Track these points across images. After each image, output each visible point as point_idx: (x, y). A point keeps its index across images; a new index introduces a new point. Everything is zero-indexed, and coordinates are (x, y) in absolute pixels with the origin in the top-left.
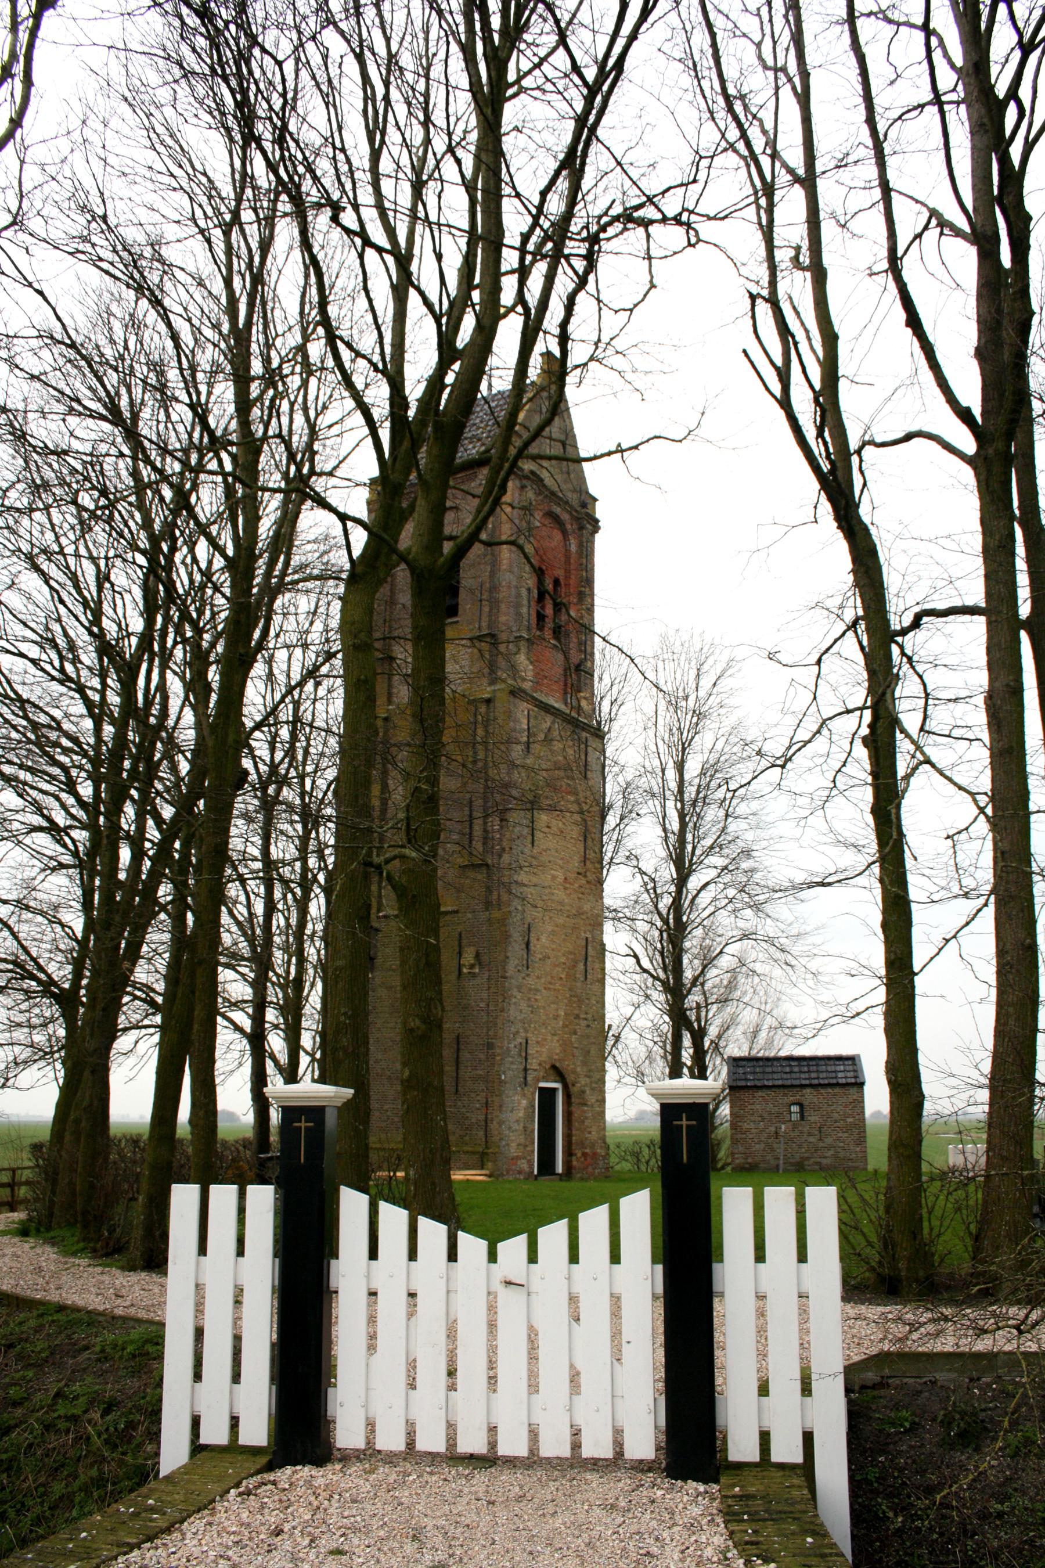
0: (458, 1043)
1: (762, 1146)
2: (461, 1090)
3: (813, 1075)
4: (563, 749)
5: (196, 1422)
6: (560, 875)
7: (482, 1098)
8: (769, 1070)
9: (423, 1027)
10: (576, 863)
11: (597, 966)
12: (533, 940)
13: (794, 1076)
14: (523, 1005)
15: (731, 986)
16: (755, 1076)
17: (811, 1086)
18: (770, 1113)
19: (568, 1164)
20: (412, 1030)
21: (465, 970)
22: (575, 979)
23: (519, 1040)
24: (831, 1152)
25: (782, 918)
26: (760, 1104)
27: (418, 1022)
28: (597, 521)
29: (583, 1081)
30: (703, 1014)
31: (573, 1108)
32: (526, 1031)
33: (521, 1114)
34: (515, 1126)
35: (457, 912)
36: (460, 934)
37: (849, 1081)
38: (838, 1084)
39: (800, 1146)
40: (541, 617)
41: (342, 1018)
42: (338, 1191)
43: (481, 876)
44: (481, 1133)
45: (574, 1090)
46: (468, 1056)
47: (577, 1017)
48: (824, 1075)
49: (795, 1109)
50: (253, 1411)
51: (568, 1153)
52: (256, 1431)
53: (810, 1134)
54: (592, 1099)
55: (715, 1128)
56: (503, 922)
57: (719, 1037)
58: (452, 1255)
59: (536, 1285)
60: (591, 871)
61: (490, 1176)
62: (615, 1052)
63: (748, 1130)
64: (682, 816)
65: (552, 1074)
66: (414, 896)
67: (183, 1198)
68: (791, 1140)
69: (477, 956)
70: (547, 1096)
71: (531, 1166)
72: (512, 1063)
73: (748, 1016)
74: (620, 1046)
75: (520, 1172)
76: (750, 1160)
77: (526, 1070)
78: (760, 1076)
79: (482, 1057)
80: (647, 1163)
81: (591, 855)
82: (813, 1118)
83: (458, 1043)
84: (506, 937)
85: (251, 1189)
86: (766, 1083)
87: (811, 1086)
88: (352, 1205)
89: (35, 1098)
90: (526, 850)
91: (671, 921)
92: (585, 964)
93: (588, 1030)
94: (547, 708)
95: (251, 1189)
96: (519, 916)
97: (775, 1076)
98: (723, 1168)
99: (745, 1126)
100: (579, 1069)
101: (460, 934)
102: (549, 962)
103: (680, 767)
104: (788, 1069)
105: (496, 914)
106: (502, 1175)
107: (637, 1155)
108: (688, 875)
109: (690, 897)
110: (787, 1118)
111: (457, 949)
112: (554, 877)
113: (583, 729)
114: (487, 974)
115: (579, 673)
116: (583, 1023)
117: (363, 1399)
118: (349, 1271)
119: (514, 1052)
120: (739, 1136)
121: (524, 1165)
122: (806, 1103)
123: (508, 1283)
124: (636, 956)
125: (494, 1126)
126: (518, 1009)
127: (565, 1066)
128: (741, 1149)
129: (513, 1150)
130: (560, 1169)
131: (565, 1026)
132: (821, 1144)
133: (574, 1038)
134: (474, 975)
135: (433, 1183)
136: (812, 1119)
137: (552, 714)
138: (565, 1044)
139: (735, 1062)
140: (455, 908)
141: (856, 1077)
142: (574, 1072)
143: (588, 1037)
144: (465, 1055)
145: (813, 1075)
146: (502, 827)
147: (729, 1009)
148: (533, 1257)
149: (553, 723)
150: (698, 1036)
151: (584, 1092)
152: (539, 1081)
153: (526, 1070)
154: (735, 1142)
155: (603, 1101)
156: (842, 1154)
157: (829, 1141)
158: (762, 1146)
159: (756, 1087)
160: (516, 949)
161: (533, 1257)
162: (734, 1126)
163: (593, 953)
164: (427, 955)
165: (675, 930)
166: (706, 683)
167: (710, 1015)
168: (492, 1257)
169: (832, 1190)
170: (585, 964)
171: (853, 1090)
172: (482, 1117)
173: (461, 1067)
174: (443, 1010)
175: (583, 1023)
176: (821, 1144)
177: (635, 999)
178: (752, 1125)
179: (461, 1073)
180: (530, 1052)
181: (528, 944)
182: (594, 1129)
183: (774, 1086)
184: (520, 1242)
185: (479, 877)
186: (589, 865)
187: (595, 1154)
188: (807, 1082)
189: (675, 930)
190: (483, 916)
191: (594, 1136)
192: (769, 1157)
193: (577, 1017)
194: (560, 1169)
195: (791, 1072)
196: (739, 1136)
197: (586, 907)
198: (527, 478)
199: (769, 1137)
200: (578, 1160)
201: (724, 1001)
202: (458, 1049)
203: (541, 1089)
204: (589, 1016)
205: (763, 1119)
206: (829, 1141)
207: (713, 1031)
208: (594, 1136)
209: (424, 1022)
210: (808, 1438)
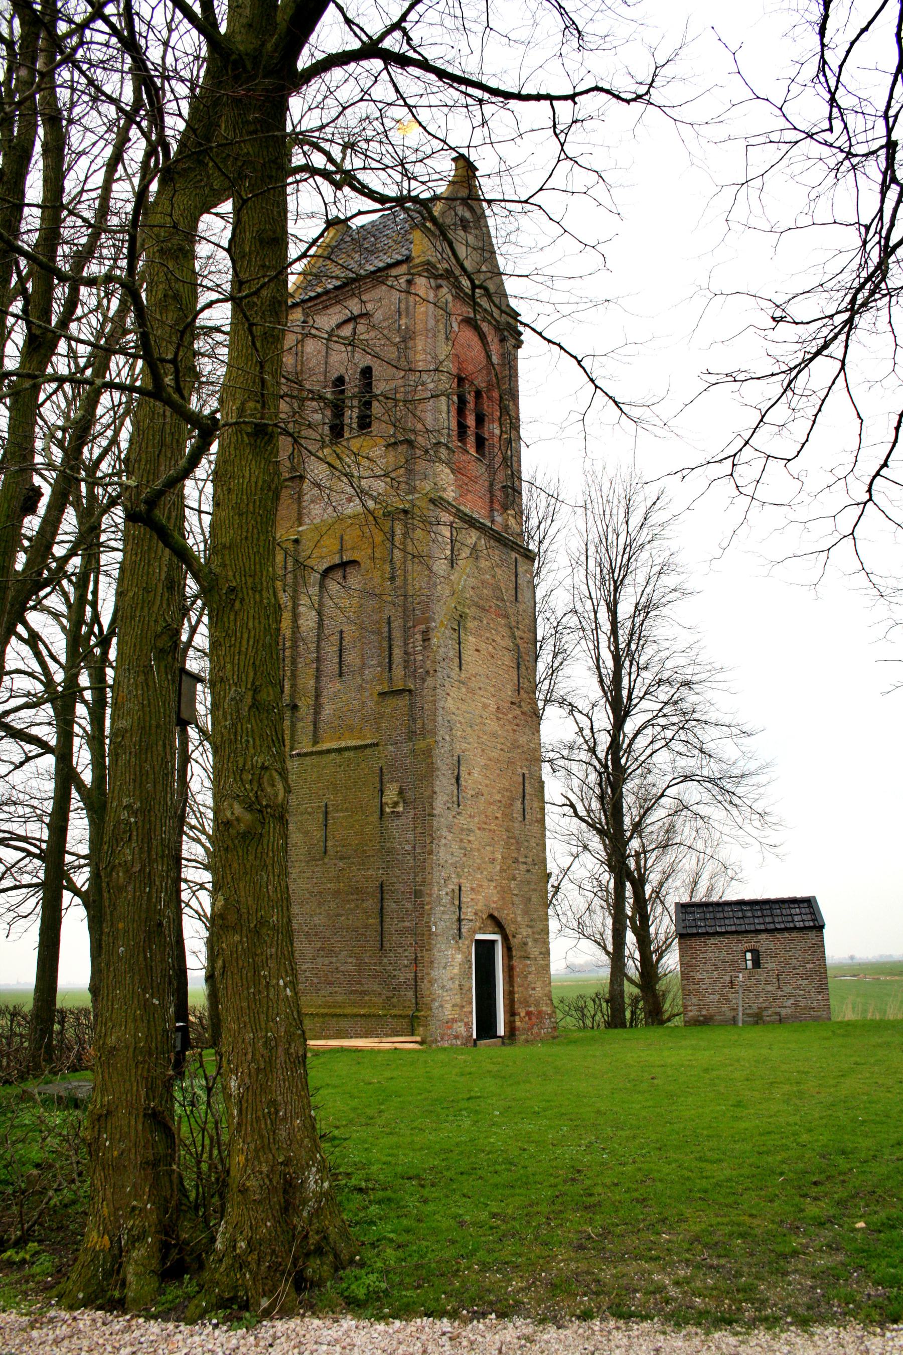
0: (382, 892)
1: (717, 997)
2: (387, 945)
3: (768, 920)
4: (493, 564)
6: (492, 704)
7: (410, 953)
8: (721, 915)
9: (248, 817)
10: (509, 692)
11: (536, 805)
12: (463, 774)
13: (747, 921)
14: (455, 846)
15: (670, 830)
16: (703, 921)
17: (766, 931)
19: (512, 1030)
20: (228, 824)
21: (388, 810)
22: (512, 819)
23: (451, 887)
24: (791, 1001)
25: (725, 757)
26: (714, 951)
27: (238, 809)
28: (522, 342)
29: (525, 931)
30: (642, 862)
31: (515, 962)
32: (459, 876)
33: (456, 971)
34: (449, 985)
35: (376, 745)
36: (381, 769)
37: (807, 924)
38: (795, 928)
39: (757, 996)
40: (462, 428)
41: (124, 815)
43: (402, 702)
44: (411, 994)
45: (514, 942)
46: (394, 906)
47: (516, 861)
48: (780, 919)
49: (749, 956)
51: (511, 1012)
53: (767, 983)
54: (534, 950)
55: (660, 979)
56: (428, 753)
57: (661, 884)
60: (525, 705)
61: (421, 1043)
62: (554, 901)
63: (701, 980)
64: (617, 658)
66: (232, 590)
69: (401, 792)
70: (485, 950)
72: (443, 912)
73: (688, 863)
74: (560, 896)
75: (456, 1037)
76: (704, 1012)
77: (459, 920)
78: (712, 923)
79: (409, 906)
80: (593, 1017)
81: (525, 684)
82: (769, 964)
83: (382, 892)
84: (432, 769)
86: (718, 929)
89: (22, 976)
90: (452, 674)
91: (609, 763)
92: (523, 803)
93: (528, 876)
94: (471, 522)
96: (447, 747)
97: (727, 922)
98: (669, 1020)
100: (519, 919)
101: (381, 769)
103: (613, 611)
104: (740, 914)
105: (421, 745)
106: (436, 1041)
107: (581, 1009)
108: (627, 714)
109: (627, 741)
110: (743, 966)
111: (378, 785)
112: (485, 706)
113: (513, 549)
114: (412, 812)
115: (508, 490)
116: (523, 868)
119: (446, 900)
120: (692, 987)
121: (460, 1028)
122: (762, 950)
124: (572, 806)
125: (424, 985)
126: (447, 851)
128: (694, 1000)
129: (448, 1012)
130: (501, 1031)
131: (502, 870)
132: (780, 993)
133: (513, 884)
134: (398, 815)
135: (273, 1103)
136: (770, 966)
137: (477, 529)
138: (504, 891)
139: (683, 908)
140: (375, 741)
141: (813, 920)
142: (514, 922)
143: (529, 883)
144: (390, 906)
145: (768, 920)
146: (425, 648)
147: (671, 855)
149: (479, 538)
150: (639, 884)
151: (525, 944)
152: (475, 932)
153: (459, 920)
154: (687, 993)
155: (547, 953)
156: (802, 1003)
157: (787, 989)
158: (717, 997)
159: (707, 934)
160: (443, 785)
162: (685, 976)
163: (529, 794)
164: (256, 691)
165: (613, 775)
166: (636, 519)
167: (649, 864)
171: (812, 934)
172: (411, 976)
173: (387, 920)
174: (288, 790)
175: (523, 868)
176: (780, 993)
177: (574, 850)
178: (705, 975)
179: (386, 927)
180: (463, 899)
181: (458, 779)
182: (538, 985)
183: (727, 932)
185: (401, 703)
186: (524, 695)
187: (540, 1012)
188: (762, 927)
189: (613, 775)
190: (406, 747)
191: (539, 992)
192: (725, 1008)
193: (516, 861)
195: (743, 917)
196: (692, 987)
197: (522, 740)
198: (441, 276)
199: (724, 987)
200: (521, 1020)
201: (664, 847)
202: (382, 899)
203: (478, 942)
204: (529, 860)
205: (717, 968)
206: (787, 989)
207: (654, 878)
208: (539, 992)
209: (249, 808)
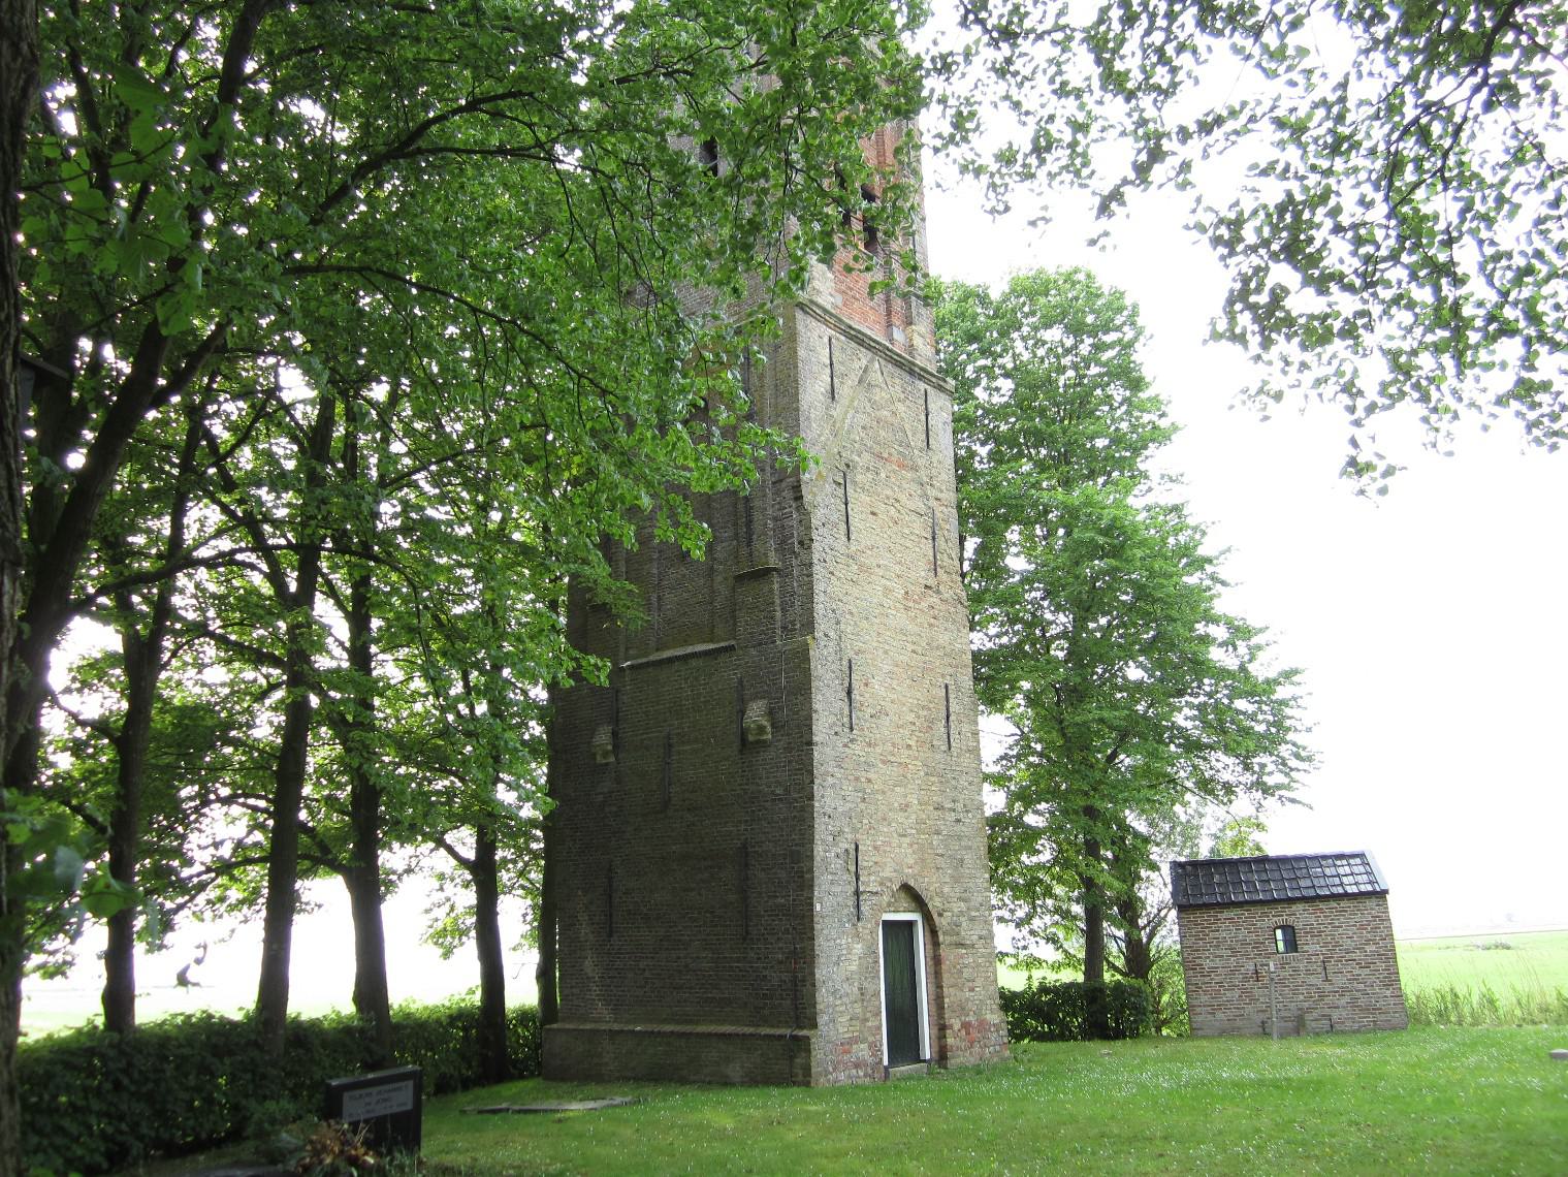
14: (848, 788)
17: (1304, 899)
18: (1244, 943)
24: (1347, 999)
26: (1230, 928)
31: (943, 951)
32: (855, 830)
37: (1363, 888)
38: (1346, 896)
42: (32, 1051)
51: (942, 1029)
63: (1214, 970)
65: (905, 902)
68: (1281, 982)
70: (900, 935)
71: (875, 1048)
77: (857, 893)
82: (1309, 945)
87: (1304, 899)
92: (948, 726)
93: (958, 828)
94: (859, 339)
99: (1207, 964)
102: (885, 721)
112: (887, 591)
116: (952, 816)
121: (862, 1051)
122: (1299, 926)
127: (927, 885)
136: (1311, 948)
137: (869, 348)
143: (960, 838)
149: (871, 361)
157: (1340, 981)
169: (292, 1010)
170: (948, 726)
171: (1371, 903)
175: (952, 816)
199: (1246, 979)
203: (885, 923)
204: (959, 806)
205: (1234, 952)
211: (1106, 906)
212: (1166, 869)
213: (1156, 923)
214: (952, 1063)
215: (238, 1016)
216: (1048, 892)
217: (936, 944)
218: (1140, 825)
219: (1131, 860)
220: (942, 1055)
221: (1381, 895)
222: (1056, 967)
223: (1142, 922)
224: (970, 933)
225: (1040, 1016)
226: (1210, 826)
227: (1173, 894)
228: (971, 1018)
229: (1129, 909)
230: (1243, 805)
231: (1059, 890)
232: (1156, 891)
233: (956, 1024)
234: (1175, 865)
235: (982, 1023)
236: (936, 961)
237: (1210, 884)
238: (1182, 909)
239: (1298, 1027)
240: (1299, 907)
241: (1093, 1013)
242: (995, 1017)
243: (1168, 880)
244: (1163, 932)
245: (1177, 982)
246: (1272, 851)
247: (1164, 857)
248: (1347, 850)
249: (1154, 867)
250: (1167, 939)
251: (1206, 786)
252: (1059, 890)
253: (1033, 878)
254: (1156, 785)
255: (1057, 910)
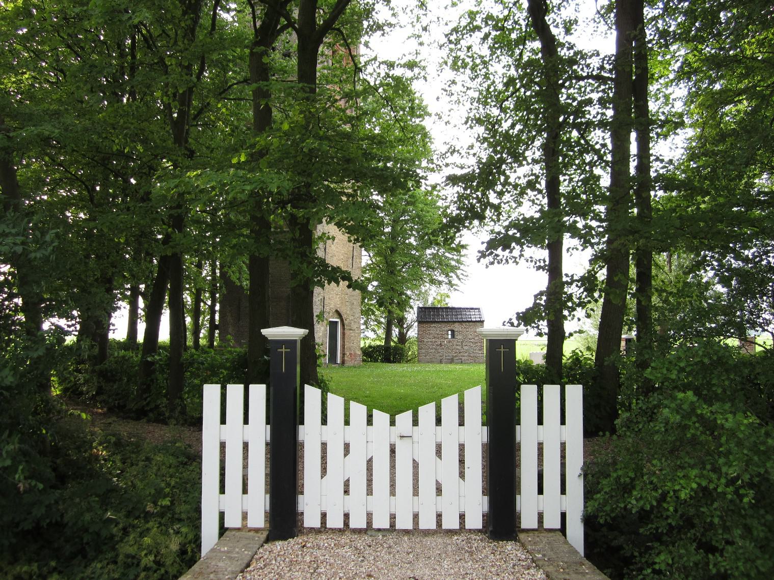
5: (222, 515)
26: (434, 329)
31: (346, 331)
38: (471, 321)
49: (450, 332)
50: (256, 507)
51: (344, 354)
52: (258, 520)
58: (370, 421)
59: (415, 438)
65: (336, 315)
67: (211, 392)
70: (333, 325)
82: (459, 337)
85: (252, 387)
87: (458, 322)
88: (312, 394)
95: (252, 387)
117: (316, 500)
118: (310, 433)
123: (402, 437)
127: (343, 311)
130: (339, 361)
148: (415, 422)
157: (466, 348)
161: (415, 422)
168: (393, 423)
184: (409, 414)
194: (339, 361)
210: (563, 516)
211: (394, 320)
212: (416, 309)
213: (409, 327)
214: (346, 365)
215: (122, 340)
216: (373, 313)
217: (344, 329)
218: (409, 292)
219: (403, 305)
220: (343, 362)
221: (482, 322)
222: (374, 340)
223: (405, 326)
224: (354, 326)
225: (370, 354)
226: (432, 294)
227: (417, 317)
228: (352, 352)
229: (401, 321)
230: (444, 288)
231: (377, 313)
232: (411, 316)
233: (348, 353)
234: (419, 308)
235: (355, 354)
236: (343, 334)
237: (429, 315)
238: (420, 322)
239: (451, 361)
240: (456, 325)
241: (388, 354)
242: (359, 352)
243: (416, 312)
244: (411, 330)
245: (415, 348)
246: (449, 305)
247: (416, 304)
248: (474, 307)
249: (411, 307)
250: (412, 333)
251: (432, 282)
252: (377, 313)
253: (369, 309)
254: (417, 279)
255: (376, 320)
